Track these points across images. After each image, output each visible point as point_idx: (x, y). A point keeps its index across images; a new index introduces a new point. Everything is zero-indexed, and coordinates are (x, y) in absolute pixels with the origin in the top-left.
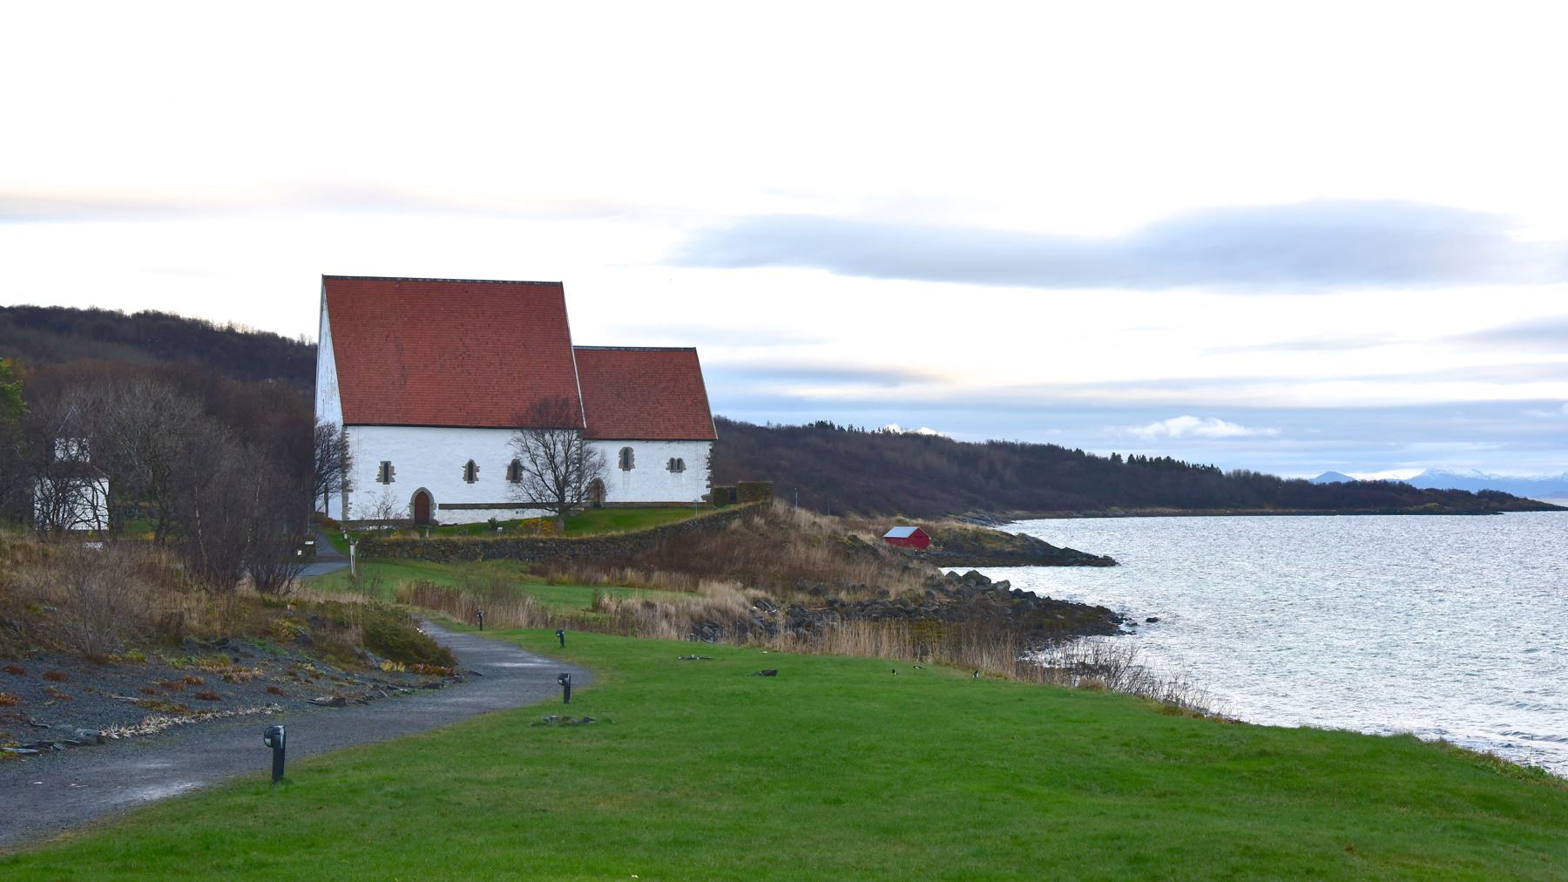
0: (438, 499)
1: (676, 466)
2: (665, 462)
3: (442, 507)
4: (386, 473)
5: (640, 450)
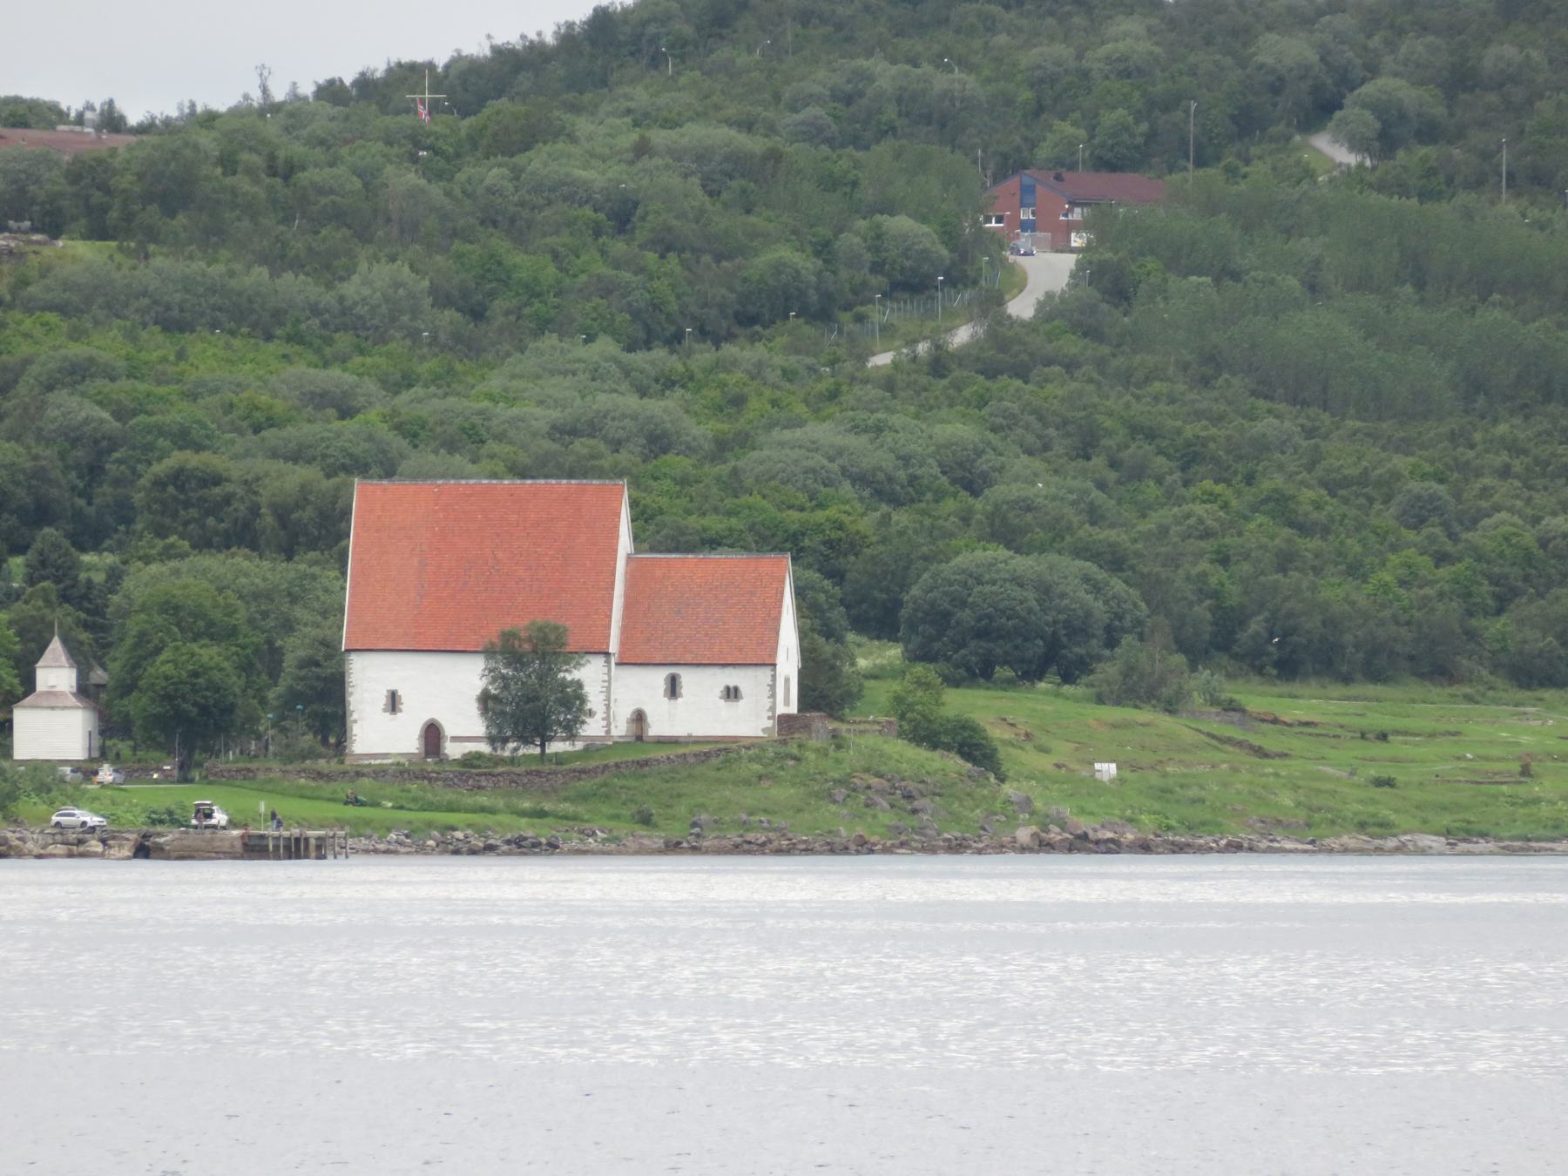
0: (449, 730)
1: (732, 694)
2: (718, 690)
3: (455, 739)
4: (394, 703)
5: (688, 677)
